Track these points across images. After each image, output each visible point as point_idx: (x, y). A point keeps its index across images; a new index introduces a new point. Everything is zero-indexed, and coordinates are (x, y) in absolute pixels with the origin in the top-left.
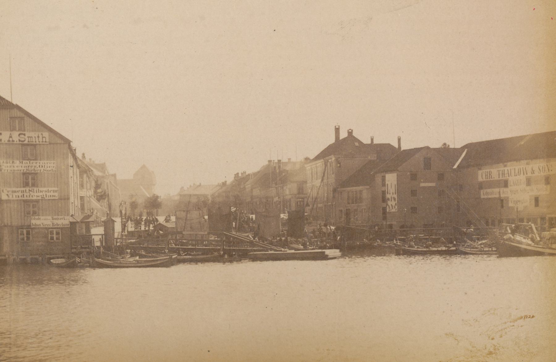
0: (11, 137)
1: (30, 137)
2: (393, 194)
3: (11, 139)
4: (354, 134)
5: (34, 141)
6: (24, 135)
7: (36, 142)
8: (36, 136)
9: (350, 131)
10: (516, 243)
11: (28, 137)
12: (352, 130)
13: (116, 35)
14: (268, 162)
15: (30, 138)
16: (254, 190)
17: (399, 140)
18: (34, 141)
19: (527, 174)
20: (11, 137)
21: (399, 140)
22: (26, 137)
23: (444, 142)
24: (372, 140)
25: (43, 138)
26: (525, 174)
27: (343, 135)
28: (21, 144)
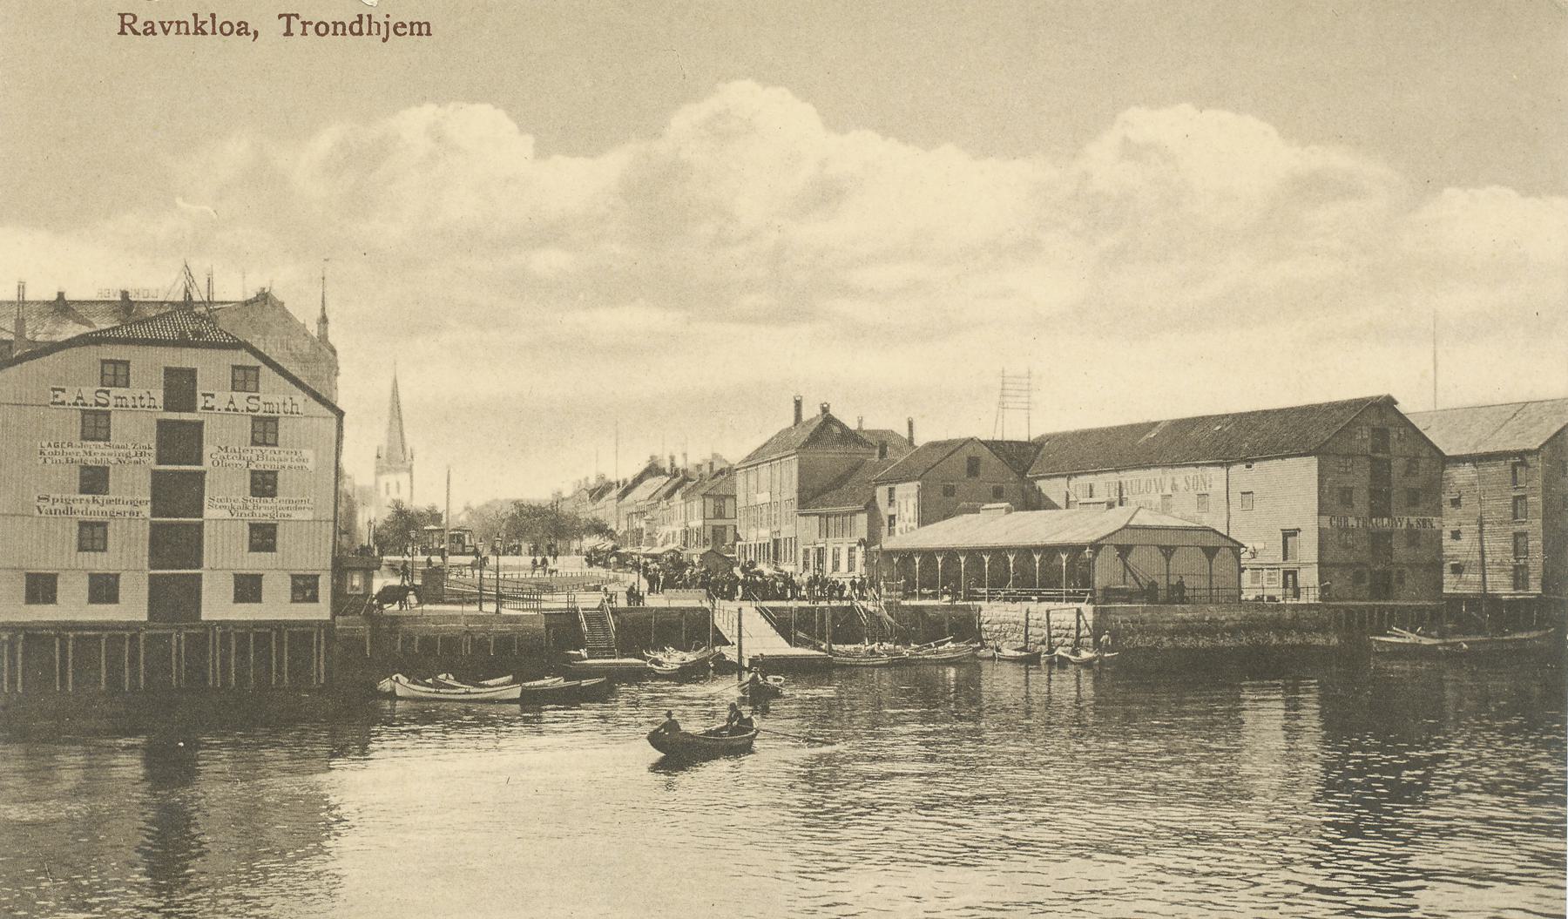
0: (231, 402)
1: (119, 397)
2: (910, 521)
3: (231, 407)
4: (831, 412)
5: (275, 410)
6: (258, 398)
7: (278, 412)
8: (281, 402)
9: (825, 406)
10: (451, 603)
11: (116, 398)
12: (829, 406)
13: (1241, 272)
14: (711, 455)
15: (119, 400)
16: (1289, 539)
17: (910, 425)
18: (275, 410)
19: (1162, 491)
20: (231, 402)
21: (910, 425)
22: (260, 403)
23: (344, 410)
24: (860, 422)
25: (292, 405)
26: (1160, 491)
27: (811, 412)
28: (252, 416)
